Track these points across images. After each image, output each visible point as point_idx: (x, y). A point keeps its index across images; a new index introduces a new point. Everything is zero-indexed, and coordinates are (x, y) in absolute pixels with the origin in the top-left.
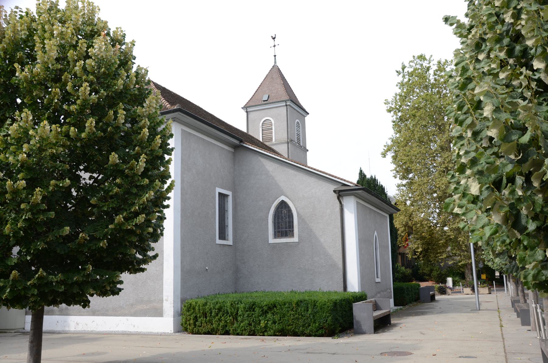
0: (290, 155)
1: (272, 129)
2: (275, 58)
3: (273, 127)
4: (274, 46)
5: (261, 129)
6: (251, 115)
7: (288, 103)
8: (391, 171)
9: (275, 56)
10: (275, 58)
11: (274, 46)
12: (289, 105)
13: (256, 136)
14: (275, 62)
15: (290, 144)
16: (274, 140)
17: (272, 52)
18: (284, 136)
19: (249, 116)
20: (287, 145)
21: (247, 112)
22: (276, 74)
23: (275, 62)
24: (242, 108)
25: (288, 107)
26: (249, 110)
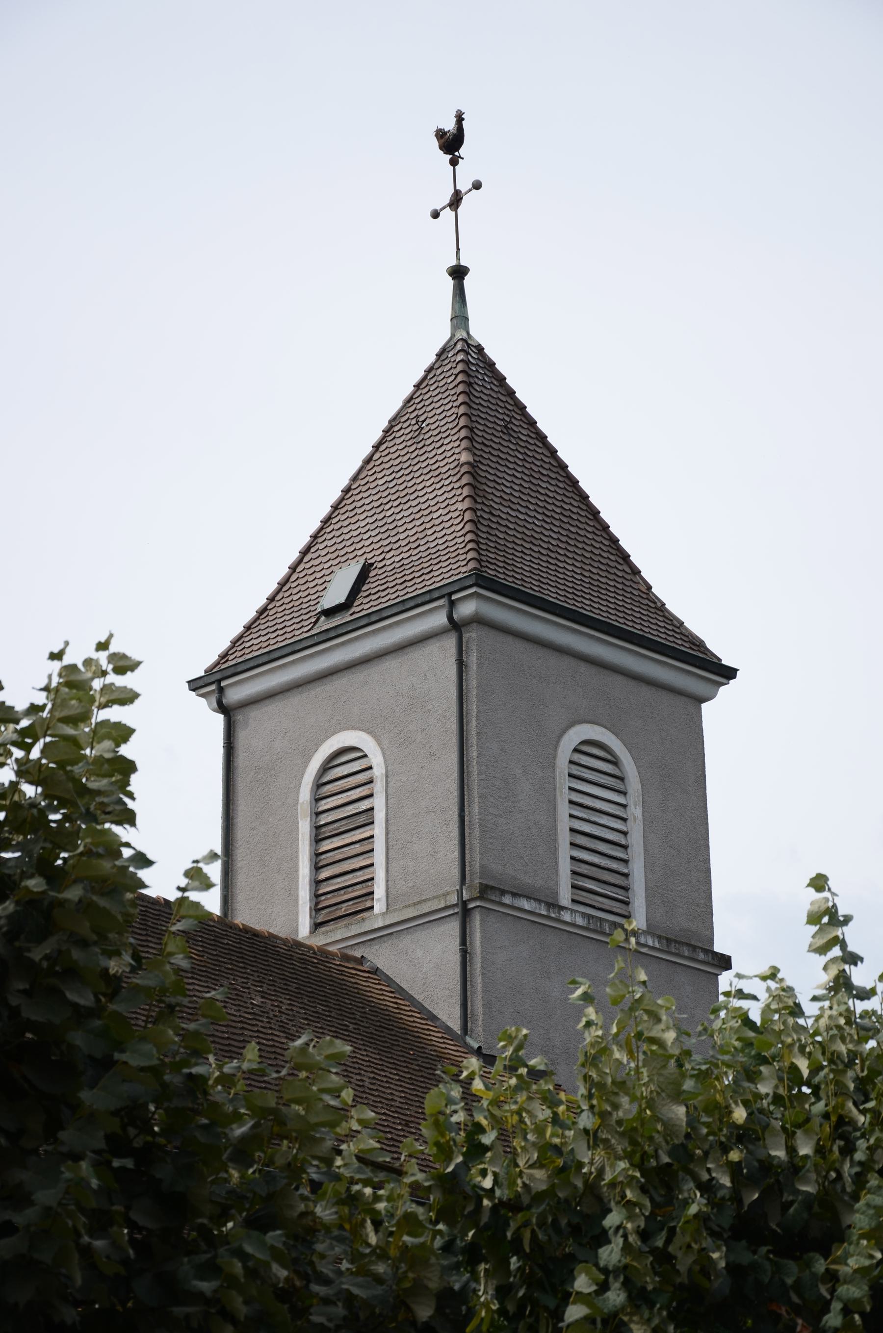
0: (478, 1005)
1: (367, 818)
2: (460, 294)
3: (379, 803)
4: (456, 201)
5: (305, 828)
6: (257, 728)
7: (467, 609)
8: (828, 921)
9: (458, 273)
10: (460, 294)
11: (456, 201)
12: (478, 620)
13: (278, 928)
14: (460, 318)
15: (477, 920)
16: (379, 906)
17: (481, 234)
18: (438, 868)
19: (242, 737)
20: (453, 927)
21: (222, 708)
22: (474, 414)
23: (460, 318)
24: (195, 685)
25: (471, 634)
26: (235, 695)
